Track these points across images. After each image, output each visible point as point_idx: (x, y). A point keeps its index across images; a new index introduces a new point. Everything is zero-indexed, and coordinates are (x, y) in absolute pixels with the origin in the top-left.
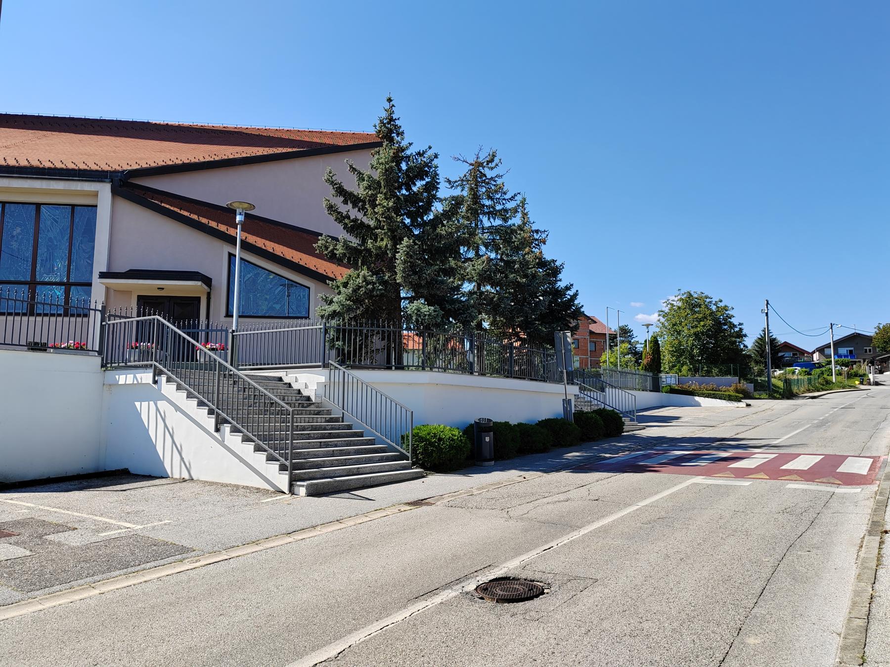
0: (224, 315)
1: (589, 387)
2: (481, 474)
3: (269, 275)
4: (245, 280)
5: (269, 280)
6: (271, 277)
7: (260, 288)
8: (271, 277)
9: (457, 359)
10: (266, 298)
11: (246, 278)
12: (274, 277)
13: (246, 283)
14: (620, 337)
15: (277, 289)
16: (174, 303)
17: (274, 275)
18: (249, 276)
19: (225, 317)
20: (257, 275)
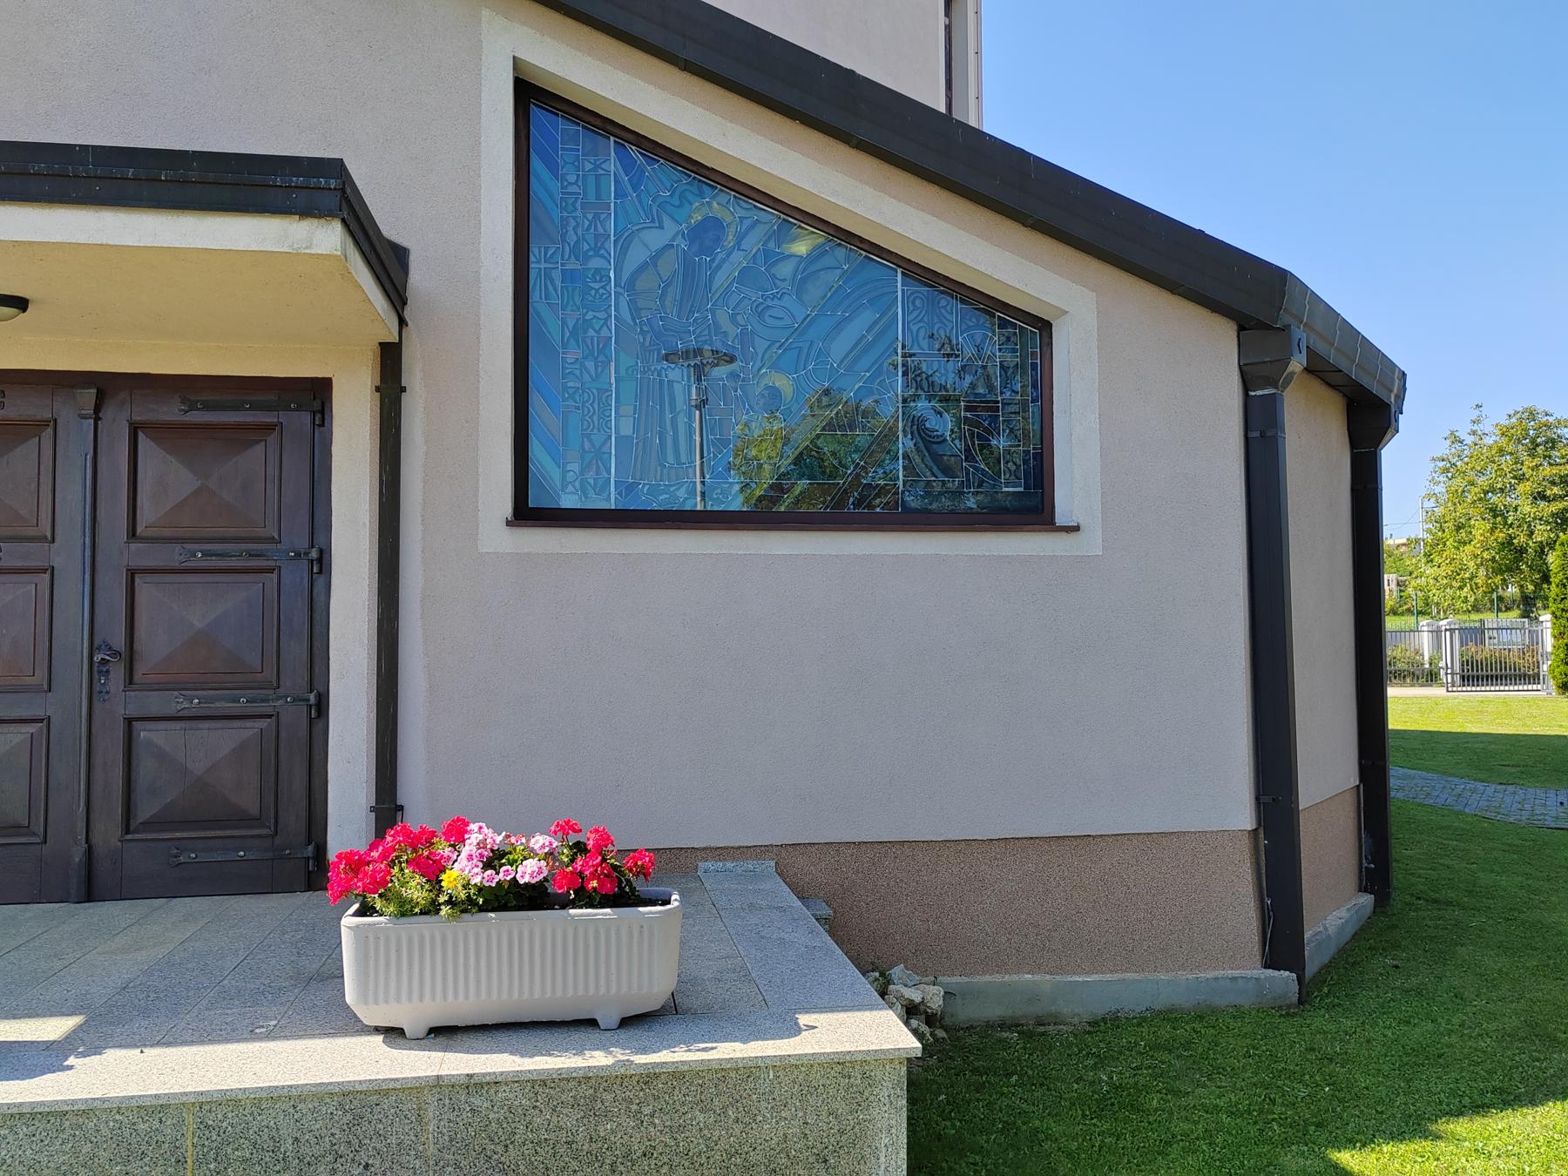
0: (507, 509)
1: (901, 461)
2: (177, 149)
3: (781, 235)
4: (625, 277)
5: (785, 270)
6: (801, 248)
7: (733, 318)
8: (801, 248)
9: (1412, 645)
10: (774, 393)
11: (637, 256)
12: (816, 255)
13: (640, 285)
14: (1028, 400)
15: (838, 327)
16: (135, 429)
17: (819, 238)
18: (654, 239)
19: (509, 524)
20: (706, 234)
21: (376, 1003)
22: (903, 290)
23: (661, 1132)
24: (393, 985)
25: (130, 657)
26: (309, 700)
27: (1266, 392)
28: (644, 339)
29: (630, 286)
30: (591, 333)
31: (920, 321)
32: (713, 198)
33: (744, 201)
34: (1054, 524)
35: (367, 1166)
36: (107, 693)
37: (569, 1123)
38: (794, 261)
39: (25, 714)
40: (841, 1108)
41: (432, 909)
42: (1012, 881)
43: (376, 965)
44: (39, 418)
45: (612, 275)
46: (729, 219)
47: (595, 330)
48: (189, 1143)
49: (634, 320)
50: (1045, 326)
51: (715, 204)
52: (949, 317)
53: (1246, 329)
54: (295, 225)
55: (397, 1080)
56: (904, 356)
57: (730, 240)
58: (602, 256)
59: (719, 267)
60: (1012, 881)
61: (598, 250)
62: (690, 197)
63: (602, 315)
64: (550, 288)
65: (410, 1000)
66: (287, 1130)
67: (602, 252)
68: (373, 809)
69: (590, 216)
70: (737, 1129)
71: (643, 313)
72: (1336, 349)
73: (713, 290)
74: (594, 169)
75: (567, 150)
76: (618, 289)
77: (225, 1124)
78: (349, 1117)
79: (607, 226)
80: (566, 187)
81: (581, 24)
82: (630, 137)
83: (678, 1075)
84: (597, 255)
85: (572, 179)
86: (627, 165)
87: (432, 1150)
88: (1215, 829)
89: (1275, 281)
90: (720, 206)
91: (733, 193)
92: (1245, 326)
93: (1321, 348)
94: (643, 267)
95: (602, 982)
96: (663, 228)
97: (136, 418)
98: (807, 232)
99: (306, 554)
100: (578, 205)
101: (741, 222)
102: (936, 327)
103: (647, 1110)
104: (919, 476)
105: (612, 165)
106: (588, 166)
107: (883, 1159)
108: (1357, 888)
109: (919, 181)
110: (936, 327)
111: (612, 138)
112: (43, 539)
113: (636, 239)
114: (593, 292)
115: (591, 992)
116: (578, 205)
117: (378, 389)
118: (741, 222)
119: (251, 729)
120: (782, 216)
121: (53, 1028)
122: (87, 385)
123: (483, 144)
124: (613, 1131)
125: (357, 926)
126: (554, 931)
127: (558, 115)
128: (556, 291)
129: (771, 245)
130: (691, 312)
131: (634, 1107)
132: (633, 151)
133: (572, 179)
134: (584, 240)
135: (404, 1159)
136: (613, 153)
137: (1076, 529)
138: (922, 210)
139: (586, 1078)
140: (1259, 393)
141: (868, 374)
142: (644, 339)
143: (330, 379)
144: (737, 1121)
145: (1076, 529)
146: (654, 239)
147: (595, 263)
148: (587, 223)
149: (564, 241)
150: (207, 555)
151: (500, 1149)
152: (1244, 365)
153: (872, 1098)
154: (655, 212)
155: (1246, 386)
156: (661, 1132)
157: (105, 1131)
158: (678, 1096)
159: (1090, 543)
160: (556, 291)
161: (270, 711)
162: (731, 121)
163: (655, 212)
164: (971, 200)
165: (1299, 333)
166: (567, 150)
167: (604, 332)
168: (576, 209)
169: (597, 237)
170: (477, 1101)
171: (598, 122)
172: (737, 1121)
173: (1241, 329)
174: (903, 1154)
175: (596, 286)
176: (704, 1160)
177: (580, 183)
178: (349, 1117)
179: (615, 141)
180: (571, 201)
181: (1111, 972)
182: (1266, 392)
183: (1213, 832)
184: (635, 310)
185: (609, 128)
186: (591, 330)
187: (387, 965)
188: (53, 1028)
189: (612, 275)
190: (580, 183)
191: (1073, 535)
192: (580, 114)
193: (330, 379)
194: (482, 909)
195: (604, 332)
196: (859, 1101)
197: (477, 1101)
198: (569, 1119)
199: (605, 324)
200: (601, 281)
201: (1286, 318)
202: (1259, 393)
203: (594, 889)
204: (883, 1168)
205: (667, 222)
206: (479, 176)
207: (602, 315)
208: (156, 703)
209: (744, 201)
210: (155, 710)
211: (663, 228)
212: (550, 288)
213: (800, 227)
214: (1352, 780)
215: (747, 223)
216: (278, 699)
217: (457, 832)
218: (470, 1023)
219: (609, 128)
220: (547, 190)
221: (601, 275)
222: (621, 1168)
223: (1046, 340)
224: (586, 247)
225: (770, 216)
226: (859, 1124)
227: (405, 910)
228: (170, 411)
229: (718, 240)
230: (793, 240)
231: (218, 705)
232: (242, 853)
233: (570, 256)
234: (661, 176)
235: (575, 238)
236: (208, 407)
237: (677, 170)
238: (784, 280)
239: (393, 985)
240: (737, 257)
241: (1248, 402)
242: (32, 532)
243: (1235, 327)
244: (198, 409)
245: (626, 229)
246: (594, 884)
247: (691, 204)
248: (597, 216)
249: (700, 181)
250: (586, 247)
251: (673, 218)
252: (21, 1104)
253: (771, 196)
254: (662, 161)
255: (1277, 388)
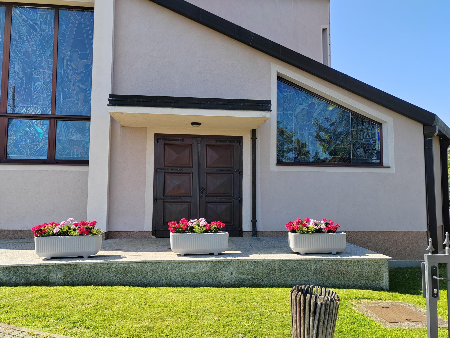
4: (296, 114)
6: (331, 108)
8: (331, 108)
11: (298, 110)
12: (334, 110)
18: (302, 107)
21: (298, 248)
22: (351, 117)
23: (349, 270)
24: (301, 245)
25: (206, 189)
26: (239, 199)
27: (429, 139)
28: (299, 127)
29: (297, 116)
30: (289, 126)
31: (355, 124)
32: (313, 98)
33: (319, 99)
34: (383, 166)
35: (303, 273)
36: (202, 197)
37: (334, 268)
38: (329, 112)
39: (188, 201)
40: (378, 268)
41: (308, 232)
42: (377, 240)
43: (298, 242)
44: (190, 144)
45: (293, 114)
46: (316, 102)
47: (289, 125)
48: (276, 267)
49: (297, 123)
50: (380, 125)
51: (313, 99)
52: (361, 123)
53: (425, 126)
54: (263, 112)
55: (308, 259)
56: (352, 130)
57: (316, 107)
58: (291, 110)
59: (314, 113)
60: (377, 240)
61: (290, 109)
62: (309, 98)
63: (291, 122)
64: (281, 117)
65: (303, 248)
66: (291, 266)
67: (291, 110)
68: (252, 221)
69: (289, 102)
70: (361, 270)
71: (299, 122)
72: (442, 129)
73: (313, 117)
74: (289, 93)
75: (284, 89)
76: (294, 117)
77: (281, 265)
78: (300, 265)
79: (292, 105)
80: (284, 97)
81: (151, 1)
82: (296, 86)
83: (351, 260)
84: (290, 110)
85: (285, 95)
86: (296, 92)
87: (313, 271)
88: (419, 231)
89: (433, 117)
90: (314, 100)
91: (317, 97)
92: (425, 125)
93: (442, 131)
94: (299, 112)
95: (334, 246)
96: (303, 105)
97: (207, 144)
98: (331, 105)
99: (238, 171)
100: (286, 100)
101: (319, 103)
102: (358, 125)
103: (346, 266)
104: (355, 156)
105: (293, 92)
106: (288, 92)
107: (385, 277)
108: (442, 248)
109: (204, 26)
110: (358, 125)
111: (293, 86)
112: (191, 167)
113: (298, 107)
114: (289, 118)
115: (336, 248)
116: (286, 100)
117: (252, 138)
118: (319, 103)
119: (229, 204)
120: (327, 102)
121: (239, 252)
122: (199, 138)
123: (271, 89)
124: (341, 270)
125: (295, 235)
126: (327, 237)
127: (282, 82)
128: (282, 118)
129: (324, 108)
130: (309, 122)
131: (344, 266)
132: (297, 89)
133: (285, 95)
134: (288, 107)
135: (309, 272)
136: (293, 89)
137: (390, 167)
138: (357, 101)
139: (336, 260)
140: (428, 139)
141: (344, 134)
142: (299, 127)
143: (242, 136)
144: (361, 269)
145: (390, 167)
146: (302, 107)
147: (290, 112)
148: (288, 104)
149: (284, 107)
150: (228, 171)
151: (323, 271)
152: (425, 133)
153: (383, 266)
154: (301, 101)
155: (425, 137)
156: (349, 270)
157: (264, 265)
158: (351, 264)
159: (392, 170)
160: (282, 118)
161: (232, 201)
162: (319, 84)
163: (301, 101)
164: (168, 8)
165: (437, 127)
166: (284, 89)
167: (291, 126)
168: (286, 101)
169: (290, 106)
170: (320, 263)
171: (290, 83)
172: (361, 269)
173: (424, 126)
174: (388, 276)
175: (290, 116)
176: (355, 275)
177: (287, 95)
178: (300, 265)
179: (294, 87)
180: (285, 99)
181: (398, 260)
182: (429, 139)
183: (418, 231)
184: (297, 121)
185: (293, 84)
186: (289, 125)
187: (300, 242)
188: (239, 252)
189: (293, 114)
190: (287, 95)
191: (388, 169)
192: (287, 82)
193: (242, 136)
194: (315, 233)
195: (291, 126)
196: (381, 267)
197: (320, 263)
198: (334, 267)
199: (292, 124)
200: (291, 115)
201: (434, 124)
202: (428, 139)
203: (333, 230)
204: (385, 278)
205: (304, 103)
206: (270, 95)
207: (291, 122)
208: (212, 199)
209: (319, 99)
210: (211, 201)
211: (303, 105)
212: (281, 117)
213: (330, 104)
214: (442, 224)
215: (320, 103)
216: (234, 199)
217: (308, 220)
218: (311, 253)
219: (293, 84)
220: (280, 97)
221: (291, 114)
222: (342, 276)
223: (381, 127)
224: (288, 109)
225: (324, 102)
226: (381, 271)
227: (304, 232)
228: (213, 142)
229: (314, 107)
230: (329, 107)
231: (223, 200)
232: (227, 229)
233: (285, 111)
234: (302, 93)
235: (286, 107)
236: (220, 142)
237: (306, 93)
238: (327, 115)
239: (301, 245)
240: (318, 110)
241: (425, 141)
242: (188, 166)
243: (423, 125)
244: (219, 142)
245: (296, 105)
246: (333, 229)
247: (309, 100)
248: (290, 102)
249: (310, 95)
250: (288, 109)
251: (305, 103)
252: (253, 259)
253: (325, 98)
254: (303, 91)
255: (432, 138)
